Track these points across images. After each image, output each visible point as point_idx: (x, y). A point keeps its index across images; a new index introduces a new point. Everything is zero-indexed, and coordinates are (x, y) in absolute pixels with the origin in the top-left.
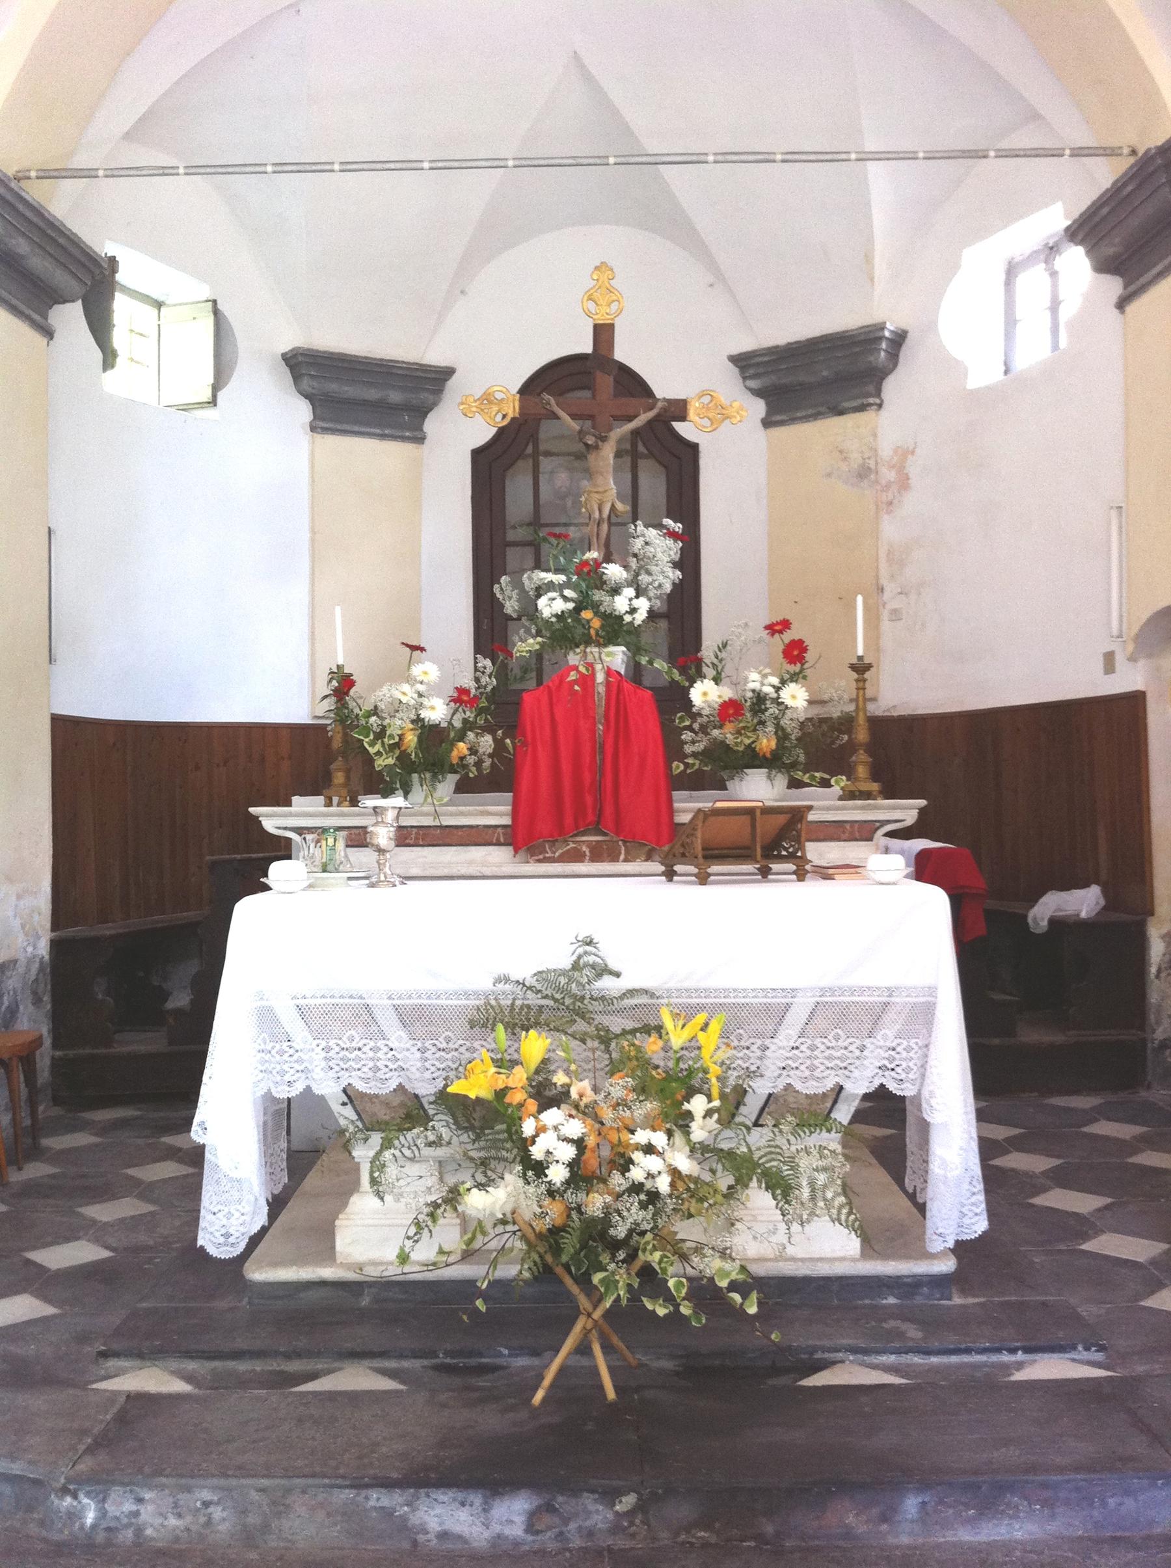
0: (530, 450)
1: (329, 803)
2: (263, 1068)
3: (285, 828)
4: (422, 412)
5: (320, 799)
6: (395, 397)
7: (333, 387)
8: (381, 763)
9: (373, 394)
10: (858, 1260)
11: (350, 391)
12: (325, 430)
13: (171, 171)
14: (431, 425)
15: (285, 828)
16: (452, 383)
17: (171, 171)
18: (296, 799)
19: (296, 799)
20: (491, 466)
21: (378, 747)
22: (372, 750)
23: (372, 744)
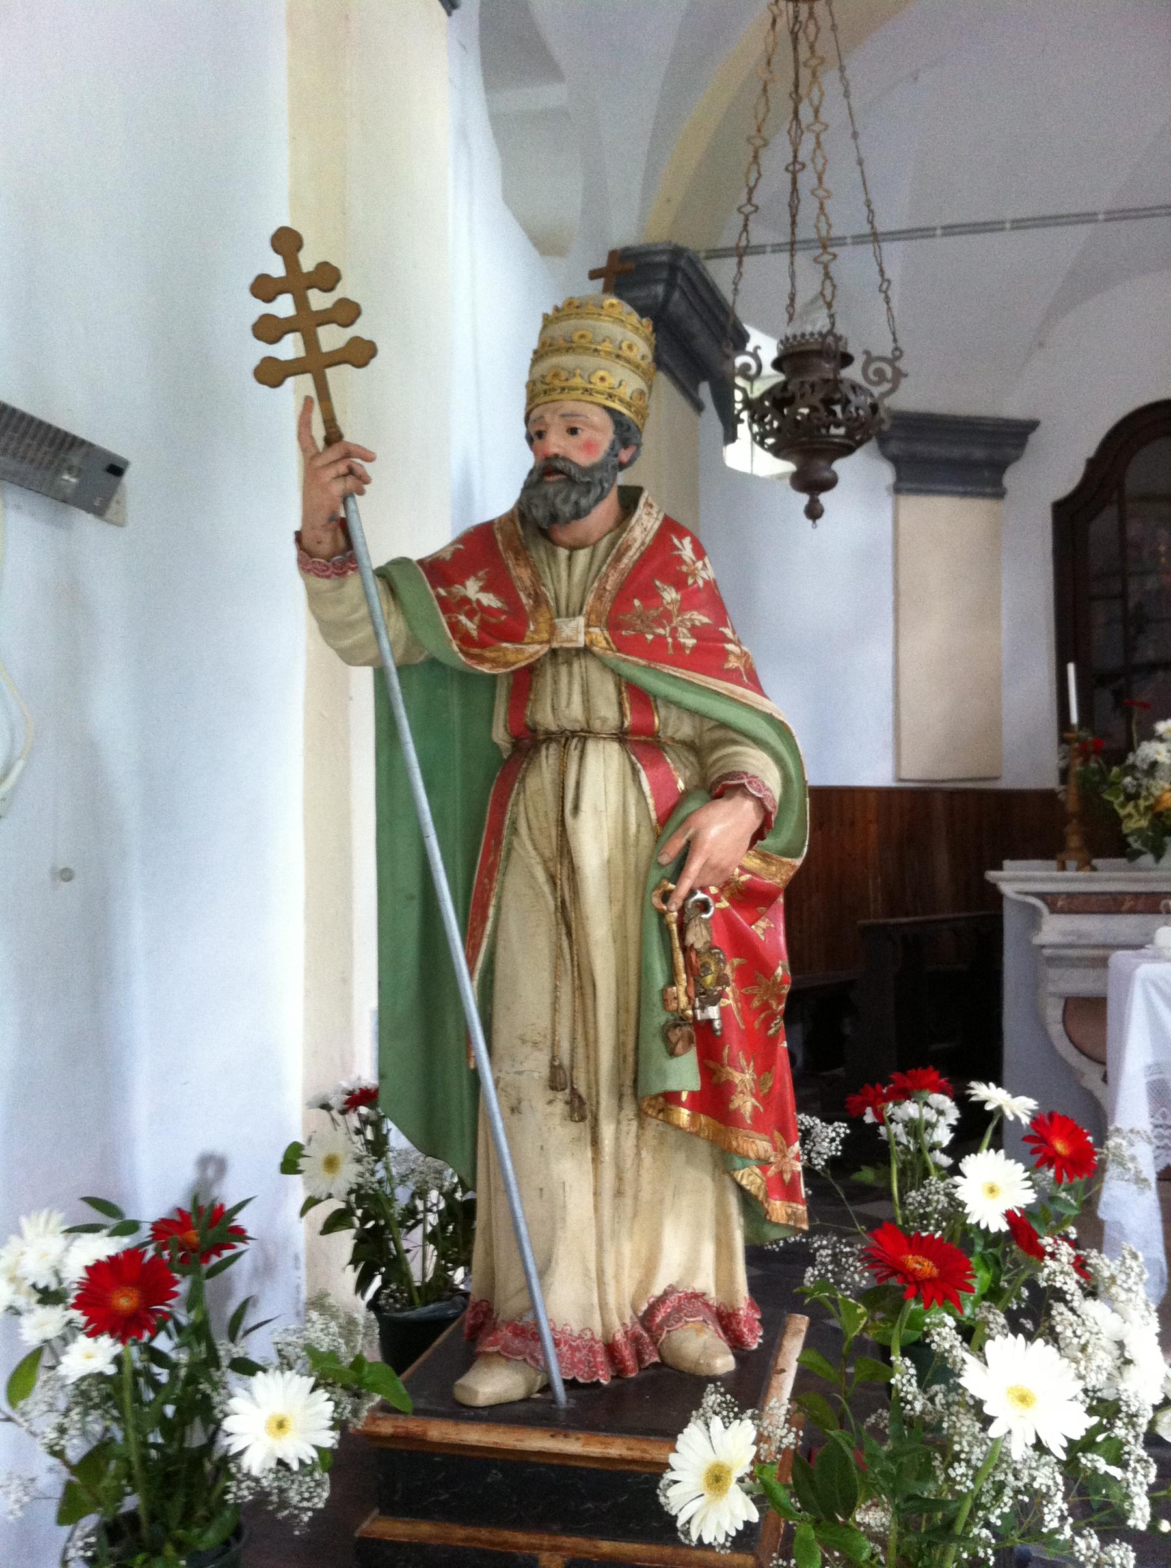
0: (1115, 496)
1: (1063, 868)
2: (1161, 1144)
3: (1027, 894)
4: (999, 467)
5: (1053, 863)
6: (979, 453)
7: (921, 448)
8: (1129, 826)
9: (956, 452)
10: (470, 1270)
11: (938, 451)
12: (910, 491)
13: (998, 226)
14: (1010, 478)
15: (1027, 894)
16: (1033, 438)
17: (998, 226)
18: (1007, 863)
19: (1007, 863)
20: (1070, 517)
21: (1130, 808)
22: (1122, 812)
23: (1123, 805)
